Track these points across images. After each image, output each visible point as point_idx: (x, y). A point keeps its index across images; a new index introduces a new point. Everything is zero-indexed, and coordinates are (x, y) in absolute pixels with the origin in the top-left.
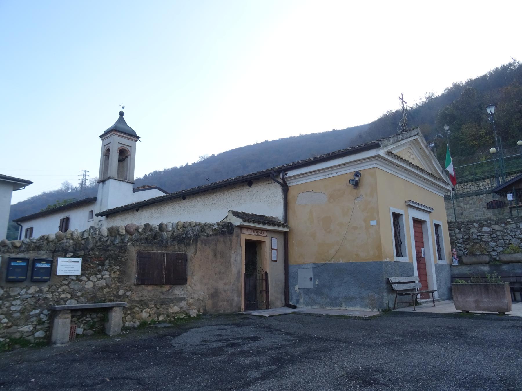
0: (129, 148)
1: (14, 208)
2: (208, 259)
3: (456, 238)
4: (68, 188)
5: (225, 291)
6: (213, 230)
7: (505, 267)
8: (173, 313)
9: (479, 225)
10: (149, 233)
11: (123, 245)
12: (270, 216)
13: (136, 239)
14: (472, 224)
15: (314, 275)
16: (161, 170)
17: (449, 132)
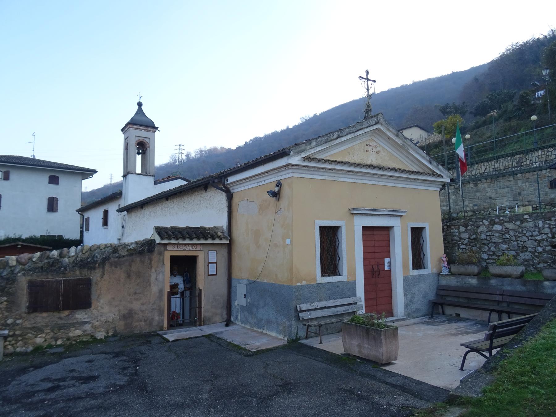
0: (147, 140)
1: (85, 196)
2: (119, 280)
3: (461, 238)
4: (176, 160)
5: (142, 311)
6: (128, 250)
7: (493, 282)
8: (74, 337)
9: (490, 222)
10: (46, 261)
11: (12, 276)
12: (212, 226)
13: (29, 268)
14: (482, 221)
15: (247, 292)
16: (262, 135)
17: (548, 78)
